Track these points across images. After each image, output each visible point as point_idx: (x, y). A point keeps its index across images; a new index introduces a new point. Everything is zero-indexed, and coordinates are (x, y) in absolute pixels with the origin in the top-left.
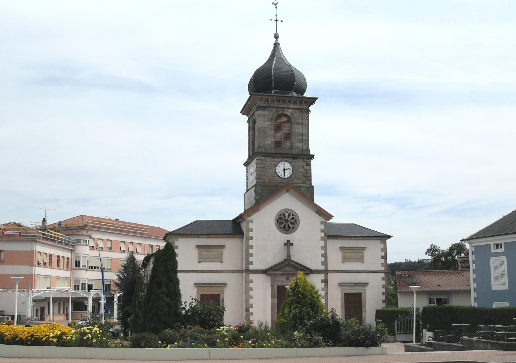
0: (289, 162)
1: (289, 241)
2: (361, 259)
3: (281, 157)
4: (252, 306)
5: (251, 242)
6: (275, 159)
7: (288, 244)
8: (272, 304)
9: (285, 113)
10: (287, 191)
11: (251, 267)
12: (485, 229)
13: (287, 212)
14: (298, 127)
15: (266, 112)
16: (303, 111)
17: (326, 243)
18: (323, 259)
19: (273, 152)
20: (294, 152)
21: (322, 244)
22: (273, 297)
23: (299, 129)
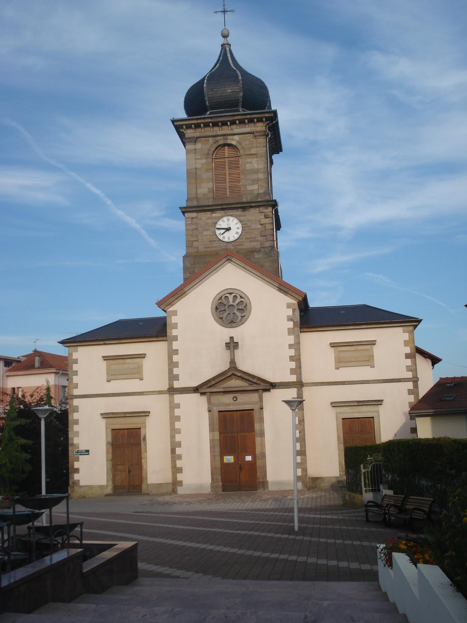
0: (232, 216)
1: (232, 338)
2: (369, 361)
3: (223, 209)
4: (179, 445)
5: (175, 345)
6: (214, 215)
7: (232, 345)
8: (212, 441)
9: (229, 142)
10: (229, 260)
11: (177, 385)
12: (250, 74)
13: (230, 294)
14: (250, 160)
15: (199, 146)
16: (256, 134)
17: (297, 338)
18: (293, 365)
19: (210, 204)
20: (244, 200)
21: (291, 339)
22: (212, 430)
23: (251, 163)
